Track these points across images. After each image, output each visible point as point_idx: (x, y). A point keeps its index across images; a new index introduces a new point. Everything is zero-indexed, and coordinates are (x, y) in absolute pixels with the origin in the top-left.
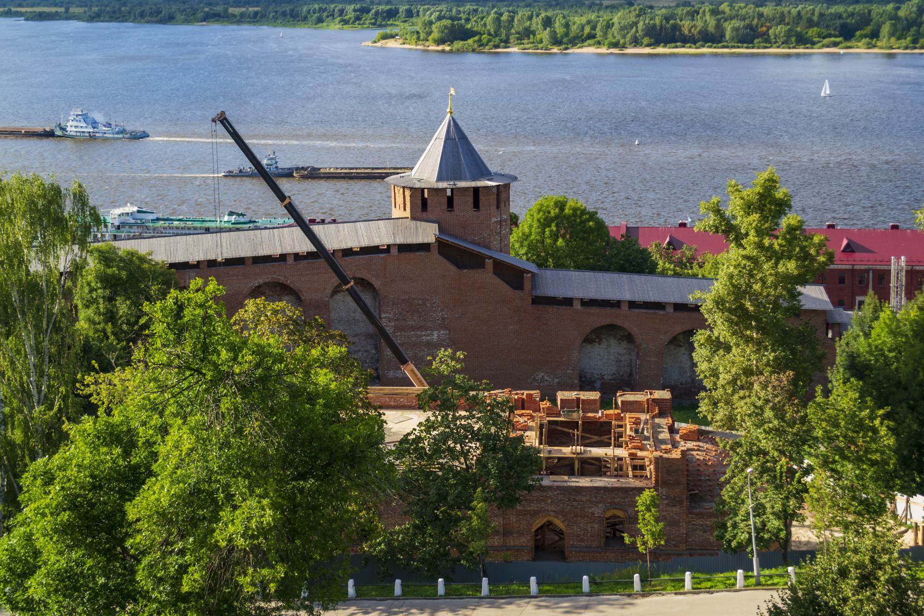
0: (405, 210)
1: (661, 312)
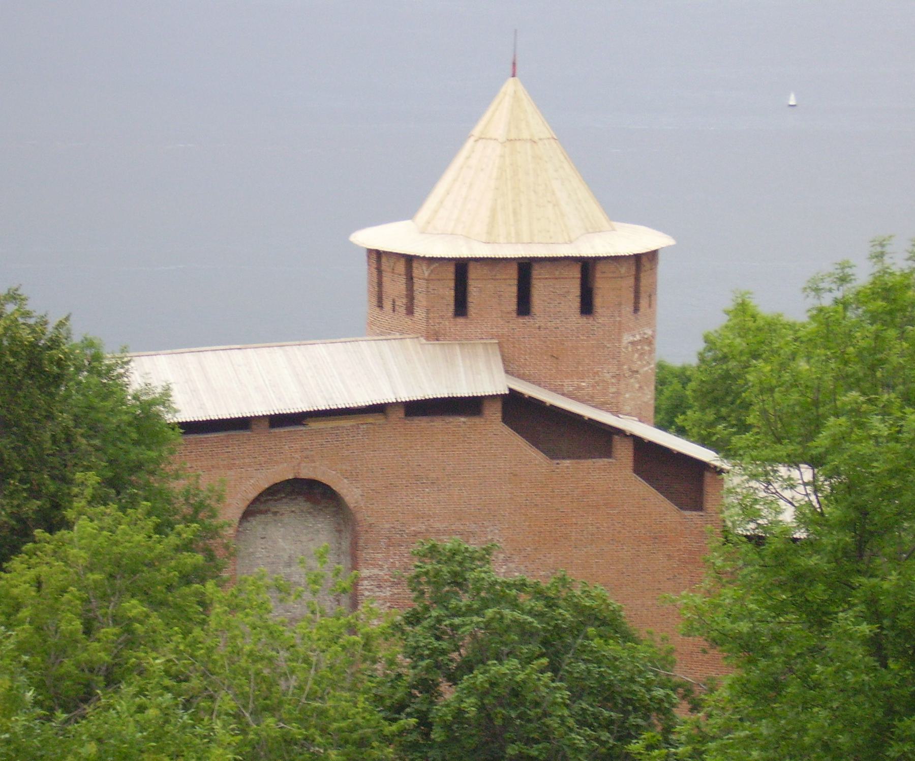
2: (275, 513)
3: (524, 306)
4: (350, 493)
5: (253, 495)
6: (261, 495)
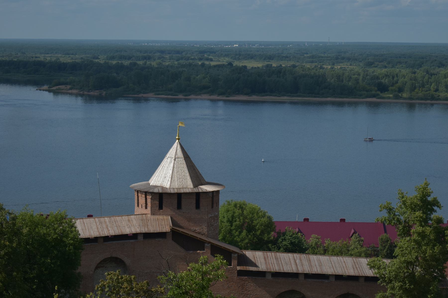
0: (146, 208)
1: (326, 281)
2: (106, 267)
3: (179, 206)
4: (128, 261)
5: (98, 262)
6: (101, 262)
